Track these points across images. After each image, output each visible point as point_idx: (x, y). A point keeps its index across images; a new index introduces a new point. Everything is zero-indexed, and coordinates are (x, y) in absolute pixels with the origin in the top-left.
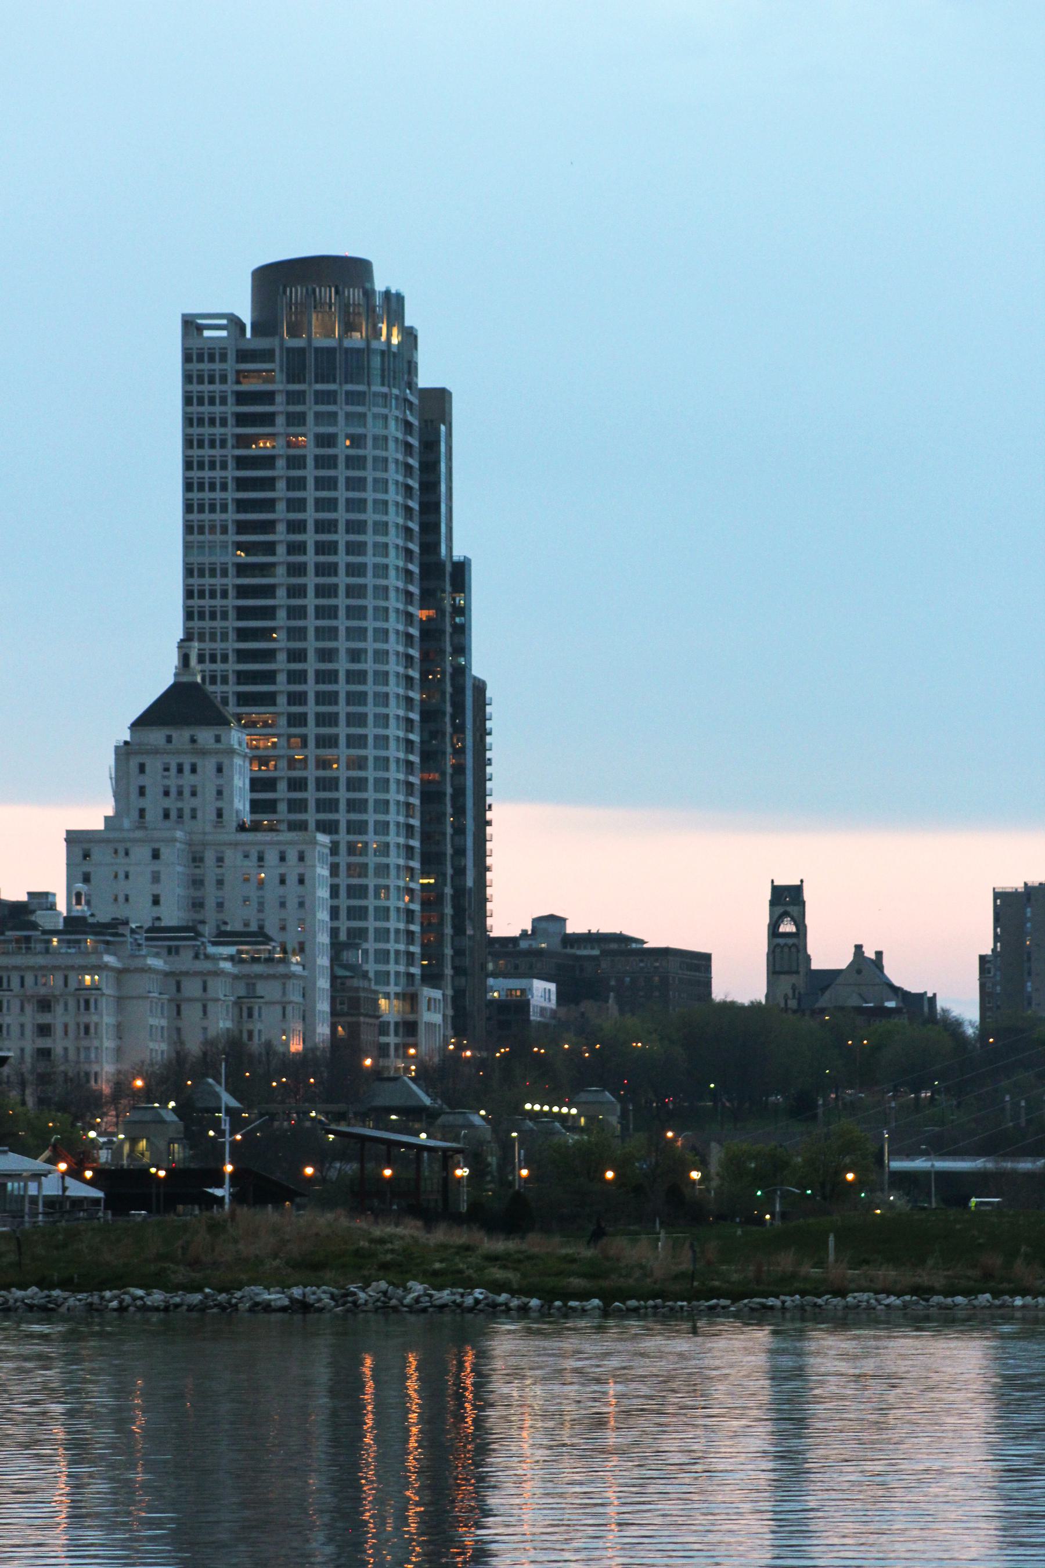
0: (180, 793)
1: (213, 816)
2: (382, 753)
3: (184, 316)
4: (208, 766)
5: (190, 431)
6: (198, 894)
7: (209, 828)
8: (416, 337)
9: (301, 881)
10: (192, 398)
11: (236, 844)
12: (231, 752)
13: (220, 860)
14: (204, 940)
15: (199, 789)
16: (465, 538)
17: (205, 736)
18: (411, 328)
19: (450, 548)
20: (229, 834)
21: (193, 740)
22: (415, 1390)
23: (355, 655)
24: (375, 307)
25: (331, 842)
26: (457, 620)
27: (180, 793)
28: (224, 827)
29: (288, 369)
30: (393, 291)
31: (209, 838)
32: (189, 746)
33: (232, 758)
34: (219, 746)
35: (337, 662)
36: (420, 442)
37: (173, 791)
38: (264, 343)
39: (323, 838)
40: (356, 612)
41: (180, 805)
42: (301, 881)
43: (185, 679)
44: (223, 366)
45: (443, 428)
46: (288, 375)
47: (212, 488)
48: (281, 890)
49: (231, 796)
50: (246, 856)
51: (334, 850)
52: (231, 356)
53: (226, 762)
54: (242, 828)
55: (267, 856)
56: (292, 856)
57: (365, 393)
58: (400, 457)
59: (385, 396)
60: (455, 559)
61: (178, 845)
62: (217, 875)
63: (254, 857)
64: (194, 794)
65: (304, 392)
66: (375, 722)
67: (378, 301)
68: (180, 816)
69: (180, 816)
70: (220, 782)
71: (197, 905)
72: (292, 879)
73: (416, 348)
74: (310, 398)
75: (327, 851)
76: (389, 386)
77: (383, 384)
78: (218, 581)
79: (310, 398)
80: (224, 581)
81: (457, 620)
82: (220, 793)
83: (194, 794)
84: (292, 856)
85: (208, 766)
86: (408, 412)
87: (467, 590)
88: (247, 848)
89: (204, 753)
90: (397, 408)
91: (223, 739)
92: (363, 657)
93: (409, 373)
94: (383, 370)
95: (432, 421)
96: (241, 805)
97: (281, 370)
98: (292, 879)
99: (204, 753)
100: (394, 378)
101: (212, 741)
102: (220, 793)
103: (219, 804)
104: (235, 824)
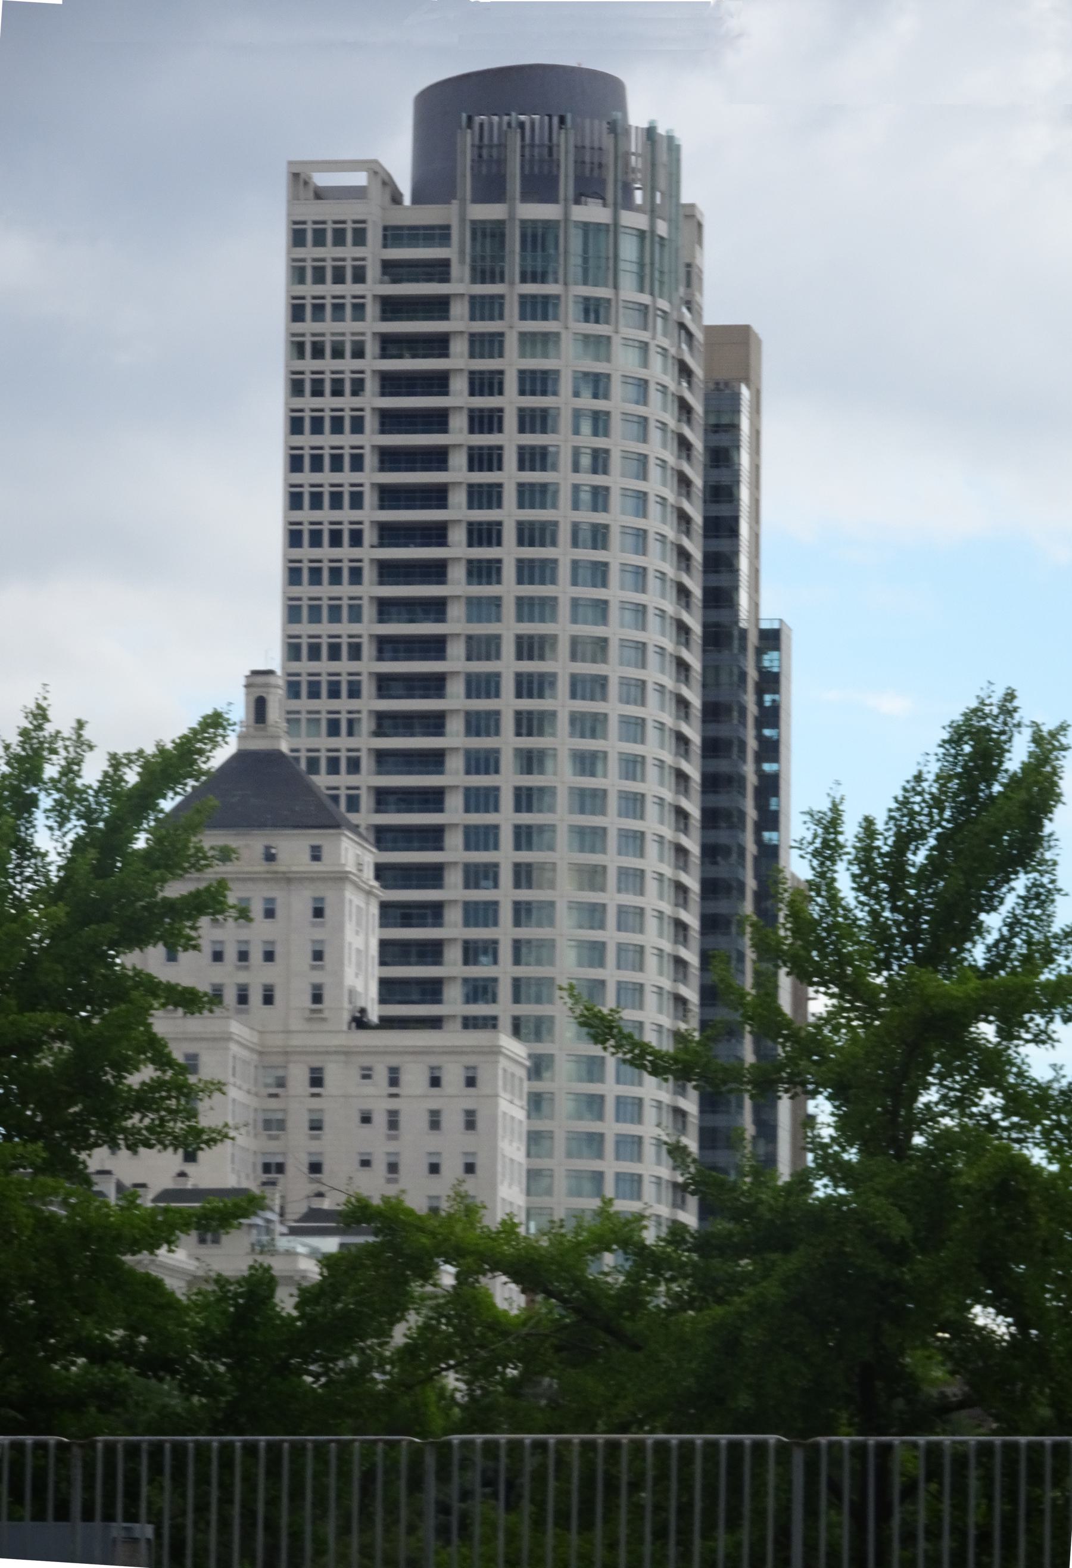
0: (243, 956)
1: (305, 1000)
2: (634, 825)
3: (291, 163)
4: (296, 905)
5: (299, 365)
6: (273, 1146)
7: (296, 1024)
8: (700, 226)
9: (470, 1122)
10: (302, 307)
11: (347, 1053)
12: (341, 878)
13: (317, 1080)
14: (269, 1215)
15: (279, 951)
16: (772, 596)
17: (293, 848)
18: (692, 206)
19: (755, 606)
20: (338, 1033)
21: (270, 857)
22: (144, 1116)
23: (587, 762)
24: (627, 154)
25: (530, 1056)
26: (767, 732)
27: (243, 956)
28: (324, 1020)
29: (474, 259)
30: (661, 130)
31: (297, 1041)
32: (262, 867)
33: (342, 890)
34: (316, 867)
35: (553, 735)
36: (705, 482)
37: (231, 954)
38: (430, 215)
39: (516, 1048)
40: (590, 725)
41: (242, 978)
42: (470, 1122)
43: (259, 744)
44: (359, 252)
45: (745, 392)
46: (473, 269)
47: (337, 464)
48: (433, 1142)
49: (341, 963)
50: (367, 1075)
51: (538, 1067)
52: (374, 236)
53: (330, 896)
54: (360, 1022)
55: (405, 1078)
56: (453, 1075)
57: (609, 301)
58: (667, 984)
59: (644, 309)
60: (764, 625)
61: (234, 1048)
62: (311, 1111)
63: (381, 1075)
64: (269, 956)
65: (502, 297)
66: (619, 881)
67: (635, 144)
68: (243, 998)
69: (243, 998)
70: (319, 934)
71: (274, 1168)
72: (453, 1120)
73: (700, 241)
74: (512, 308)
75: (522, 1073)
76: (652, 294)
77: (641, 290)
78: (345, 629)
79: (512, 308)
80: (355, 628)
81: (767, 732)
82: (318, 956)
83: (269, 956)
84: (453, 1075)
85: (296, 905)
86: (684, 346)
87: (783, 646)
88: (366, 1061)
89: (288, 879)
90: (665, 335)
91: (325, 854)
92: (599, 767)
93: (689, 285)
94: (641, 265)
95: (726, 384)
96: (360, 977)
97: (462, 261)
98: (453, 1120)
99: (288, 879)
100: (662, 283)
101: (306, 856)
102: (318, 956)
103: (317, 977)
104: (346, 1017)
